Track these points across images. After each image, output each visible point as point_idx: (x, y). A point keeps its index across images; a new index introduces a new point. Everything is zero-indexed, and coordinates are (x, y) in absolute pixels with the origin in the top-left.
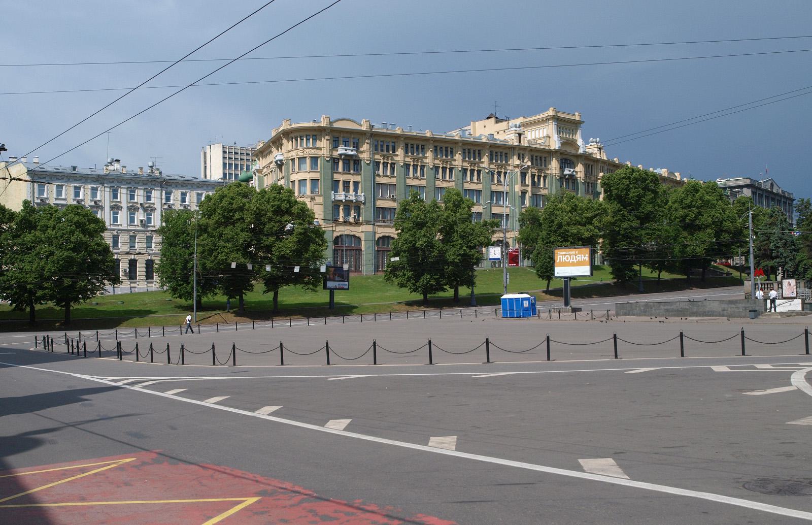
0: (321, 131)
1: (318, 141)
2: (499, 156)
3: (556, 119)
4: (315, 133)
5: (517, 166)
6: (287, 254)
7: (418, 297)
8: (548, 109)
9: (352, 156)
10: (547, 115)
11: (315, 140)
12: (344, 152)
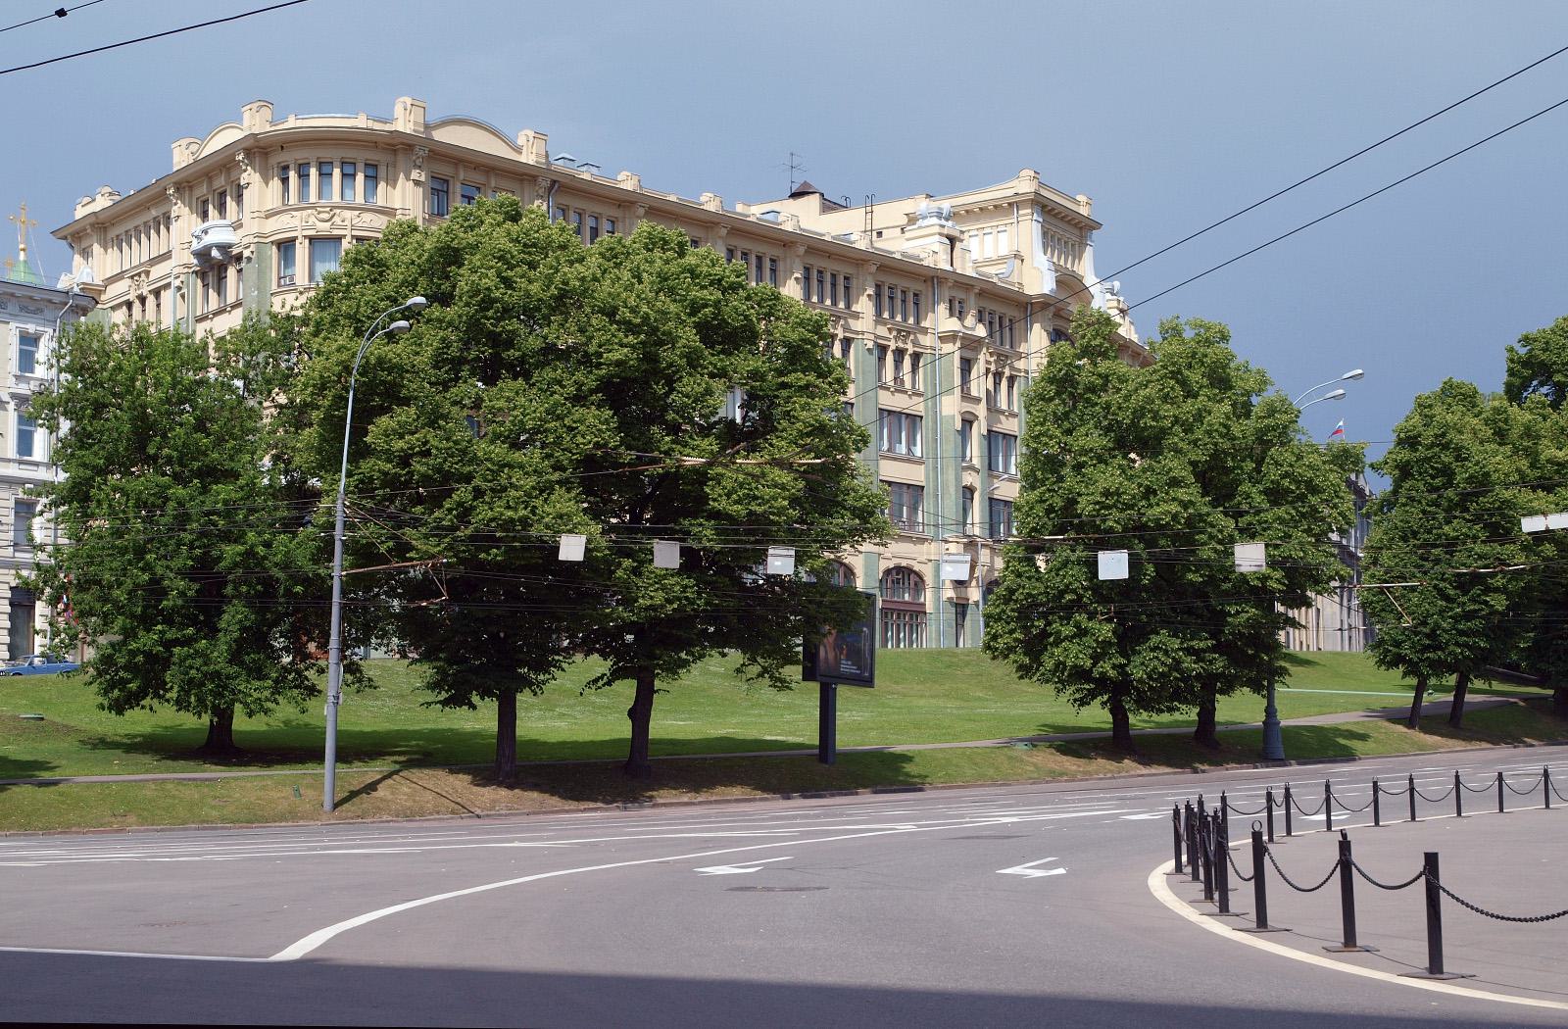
0: (395, 152)
1: (382, 186)
2: (898, 302)
3: (1041, 205)
4: (373, 156)
5: (949, 337)
6: (780, 512)
7: (1097, 716)
8: (1014, 174)
10: (1010, 192)
11: (372, 179)
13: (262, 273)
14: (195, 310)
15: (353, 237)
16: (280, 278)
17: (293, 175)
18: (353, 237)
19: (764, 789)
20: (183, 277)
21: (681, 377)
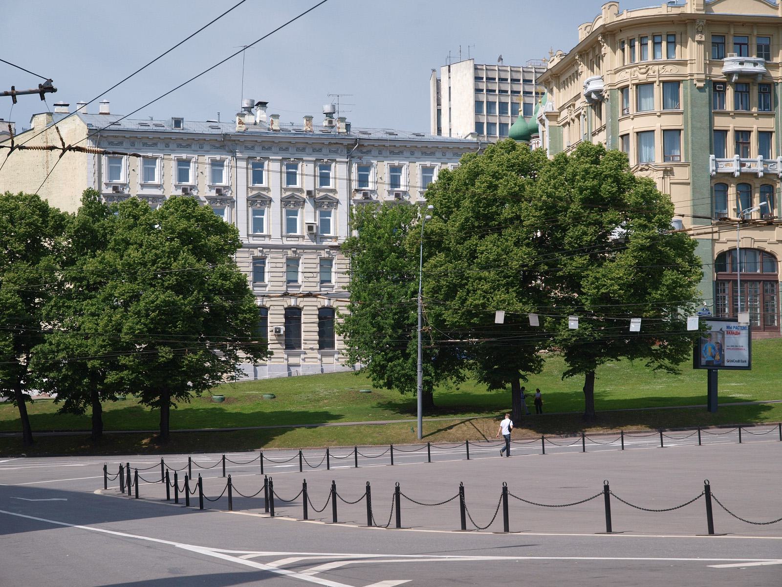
1: (678, 47)
4: (671, 29)
6: (615, 292)
9: (754, 75)
11: (672, 44)
12: (736, 67)
13: (613, 109)
14: (591, 129)
15: (660, 81)
16: (623, 110)
17: (626, 46)
18: (660, 81)
19: (651, 427)
20: (585, 109)
21: (570, 228)
